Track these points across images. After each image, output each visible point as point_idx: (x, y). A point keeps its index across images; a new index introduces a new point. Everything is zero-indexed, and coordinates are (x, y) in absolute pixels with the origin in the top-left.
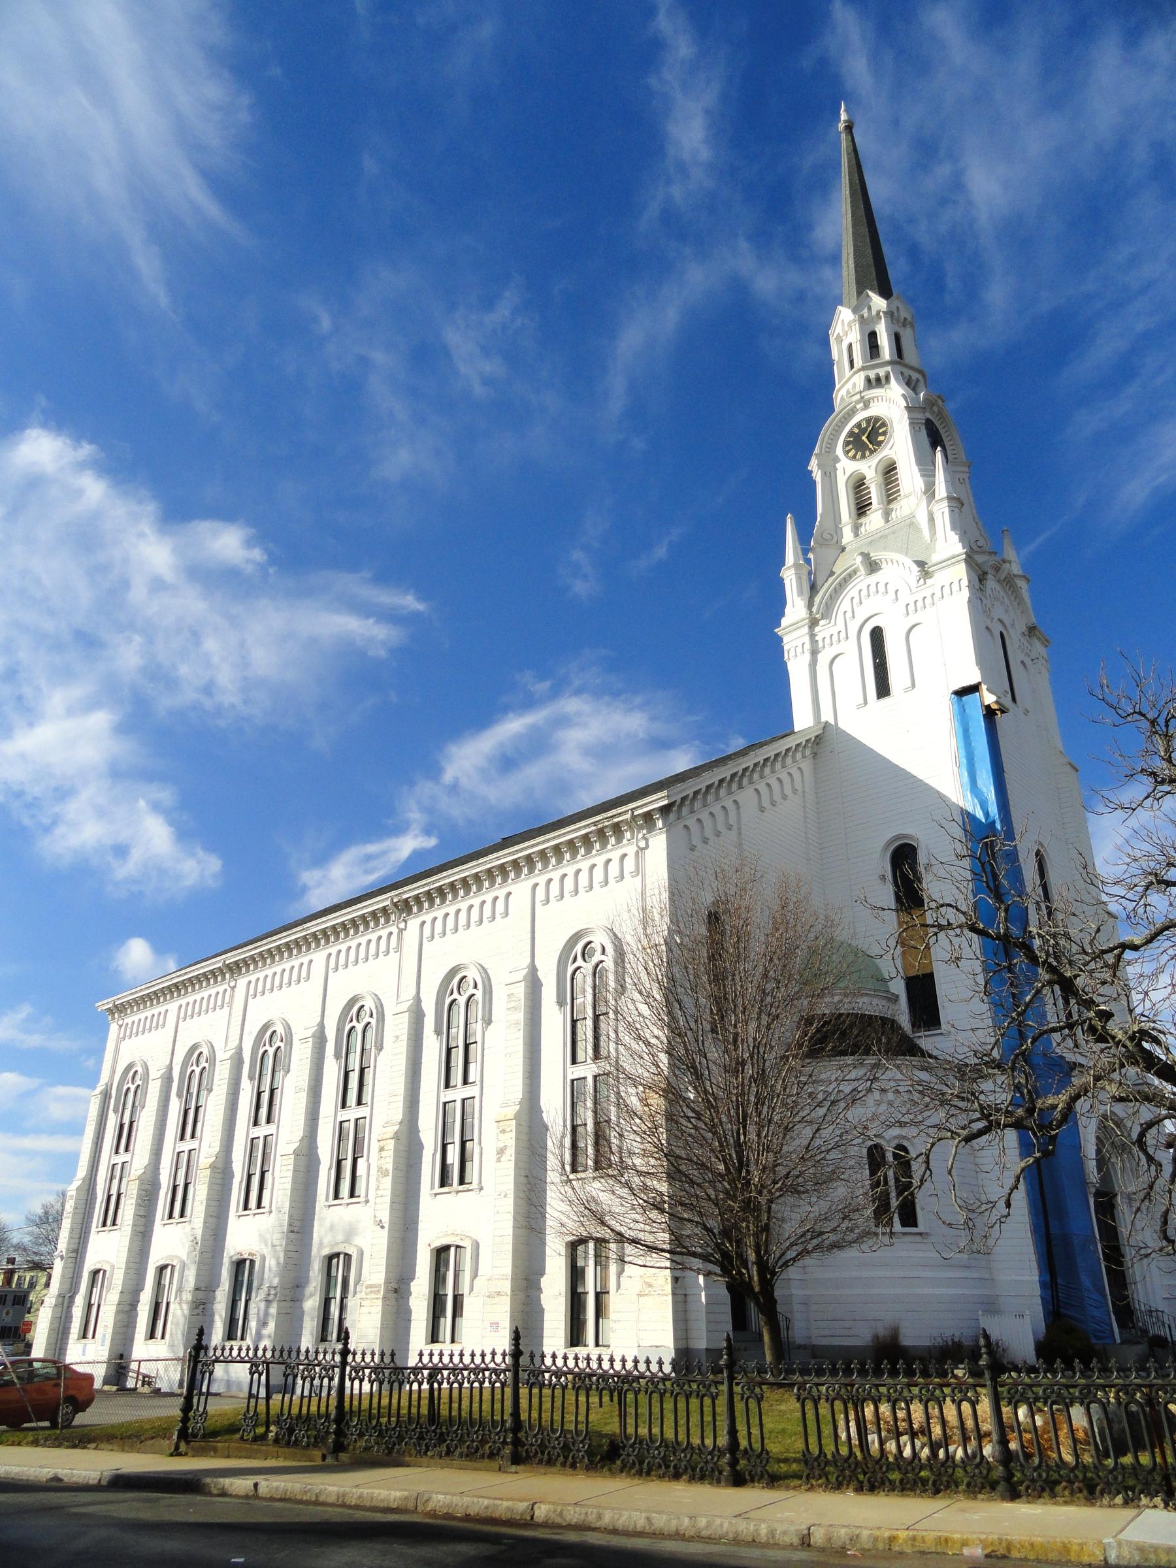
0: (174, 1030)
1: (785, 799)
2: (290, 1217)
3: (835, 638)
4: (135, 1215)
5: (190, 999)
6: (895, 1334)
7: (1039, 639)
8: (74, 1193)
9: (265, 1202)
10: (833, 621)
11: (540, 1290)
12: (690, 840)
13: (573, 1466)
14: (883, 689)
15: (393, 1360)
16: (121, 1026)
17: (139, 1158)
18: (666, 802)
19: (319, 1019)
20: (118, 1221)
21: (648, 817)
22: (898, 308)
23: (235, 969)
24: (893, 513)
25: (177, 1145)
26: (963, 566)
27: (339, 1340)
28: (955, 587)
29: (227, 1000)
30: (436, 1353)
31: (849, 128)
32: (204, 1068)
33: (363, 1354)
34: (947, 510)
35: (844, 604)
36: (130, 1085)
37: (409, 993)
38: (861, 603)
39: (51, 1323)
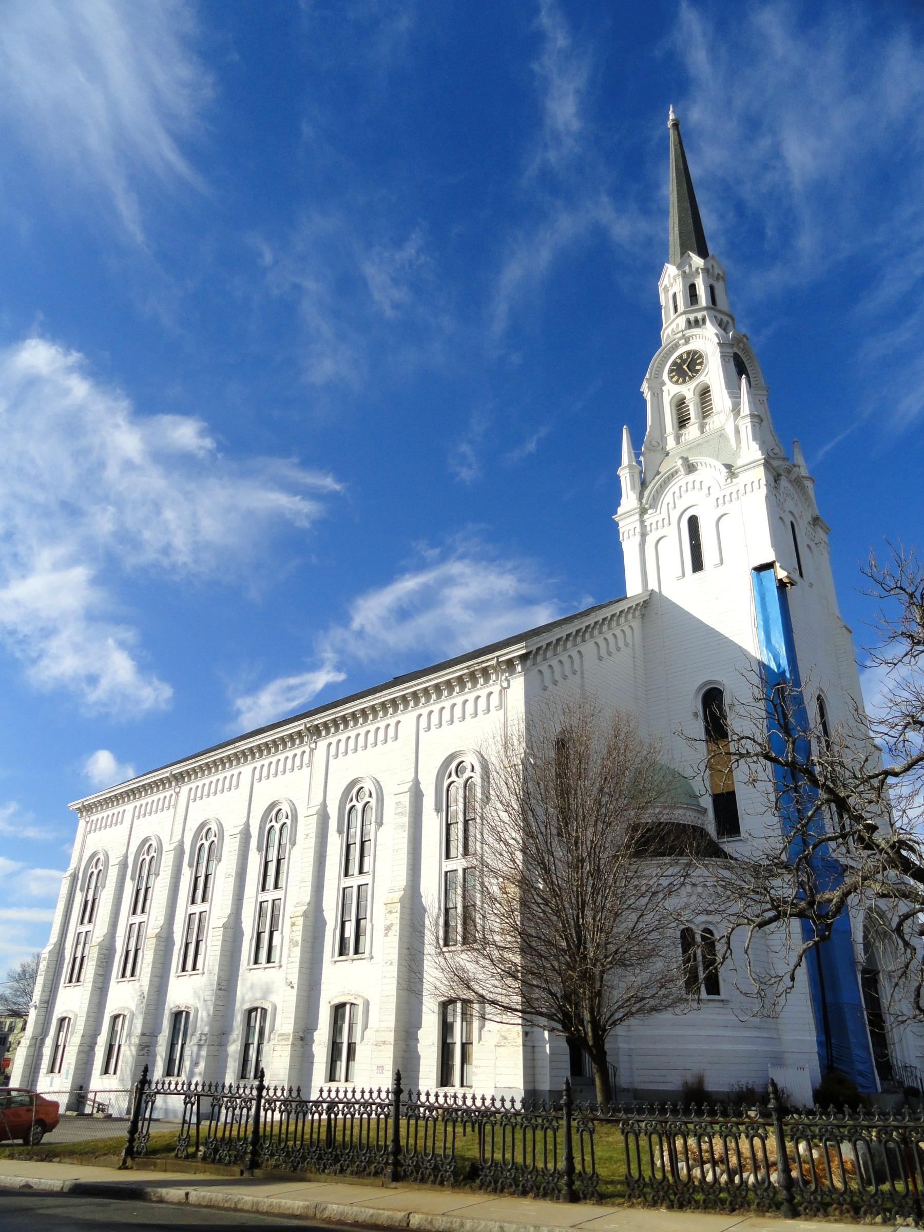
0: (129, 826)
1: (619, 651)
2: (219, 977)
3: (660, 524)
4: (96, 974)
5: (143, 801)
6: (700, 1081)
7: (822, 527)
8: (47, 955)
9: (199, 965)
10: (658, 510)
11: (417, 1040)
12: (543, 681)
13: (442, 1184)
14: (698, 565)
15: (299, 1095)
16: (87, 822)
17: (99, 929)
18: (524, 651)
19: (245, 819)
20: (82, 979)
21: (510, 663)
22: (713, 266)
23: (179, 778)
24: (707, 426)
25: (130, 918)
26: (762, 469)
27: (255, 1078)
28: (756, 485)
29: (172, 803)
30: (334, 1089)
31: (676, 125)
32: (153, 857)
33: (275, 1089)
34: (749, 425)
35: (667, 498)
36: (94, 869)
37: (317, 799)
38: (681, 497)
39: (26, 1060)
